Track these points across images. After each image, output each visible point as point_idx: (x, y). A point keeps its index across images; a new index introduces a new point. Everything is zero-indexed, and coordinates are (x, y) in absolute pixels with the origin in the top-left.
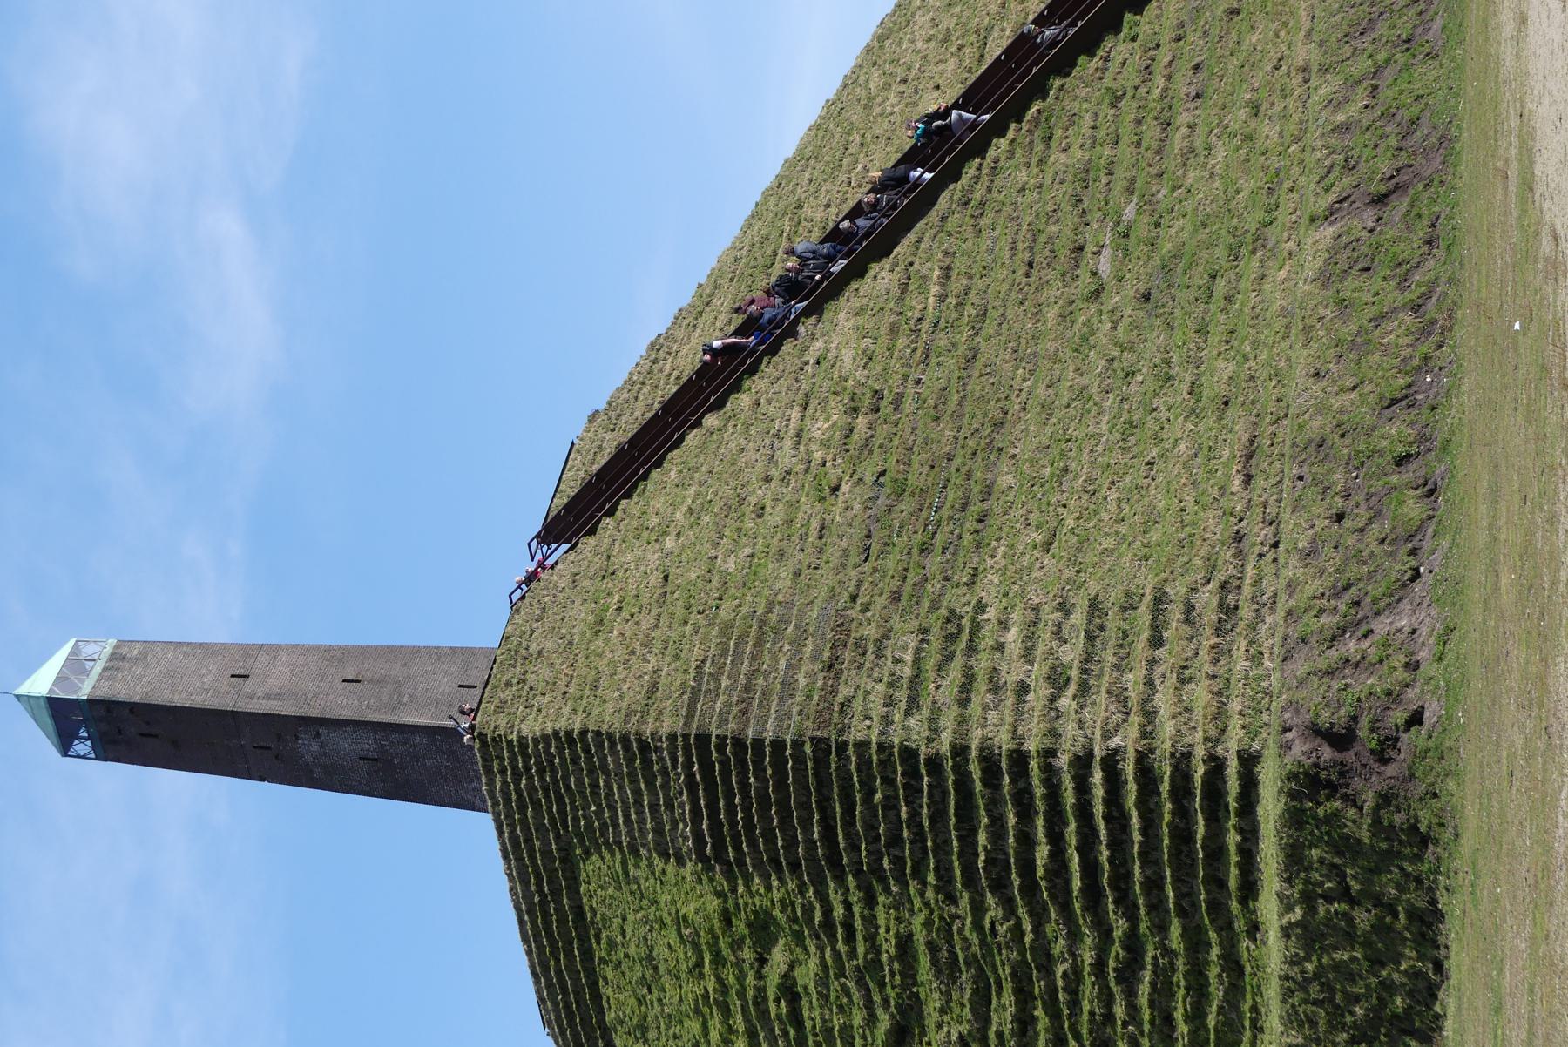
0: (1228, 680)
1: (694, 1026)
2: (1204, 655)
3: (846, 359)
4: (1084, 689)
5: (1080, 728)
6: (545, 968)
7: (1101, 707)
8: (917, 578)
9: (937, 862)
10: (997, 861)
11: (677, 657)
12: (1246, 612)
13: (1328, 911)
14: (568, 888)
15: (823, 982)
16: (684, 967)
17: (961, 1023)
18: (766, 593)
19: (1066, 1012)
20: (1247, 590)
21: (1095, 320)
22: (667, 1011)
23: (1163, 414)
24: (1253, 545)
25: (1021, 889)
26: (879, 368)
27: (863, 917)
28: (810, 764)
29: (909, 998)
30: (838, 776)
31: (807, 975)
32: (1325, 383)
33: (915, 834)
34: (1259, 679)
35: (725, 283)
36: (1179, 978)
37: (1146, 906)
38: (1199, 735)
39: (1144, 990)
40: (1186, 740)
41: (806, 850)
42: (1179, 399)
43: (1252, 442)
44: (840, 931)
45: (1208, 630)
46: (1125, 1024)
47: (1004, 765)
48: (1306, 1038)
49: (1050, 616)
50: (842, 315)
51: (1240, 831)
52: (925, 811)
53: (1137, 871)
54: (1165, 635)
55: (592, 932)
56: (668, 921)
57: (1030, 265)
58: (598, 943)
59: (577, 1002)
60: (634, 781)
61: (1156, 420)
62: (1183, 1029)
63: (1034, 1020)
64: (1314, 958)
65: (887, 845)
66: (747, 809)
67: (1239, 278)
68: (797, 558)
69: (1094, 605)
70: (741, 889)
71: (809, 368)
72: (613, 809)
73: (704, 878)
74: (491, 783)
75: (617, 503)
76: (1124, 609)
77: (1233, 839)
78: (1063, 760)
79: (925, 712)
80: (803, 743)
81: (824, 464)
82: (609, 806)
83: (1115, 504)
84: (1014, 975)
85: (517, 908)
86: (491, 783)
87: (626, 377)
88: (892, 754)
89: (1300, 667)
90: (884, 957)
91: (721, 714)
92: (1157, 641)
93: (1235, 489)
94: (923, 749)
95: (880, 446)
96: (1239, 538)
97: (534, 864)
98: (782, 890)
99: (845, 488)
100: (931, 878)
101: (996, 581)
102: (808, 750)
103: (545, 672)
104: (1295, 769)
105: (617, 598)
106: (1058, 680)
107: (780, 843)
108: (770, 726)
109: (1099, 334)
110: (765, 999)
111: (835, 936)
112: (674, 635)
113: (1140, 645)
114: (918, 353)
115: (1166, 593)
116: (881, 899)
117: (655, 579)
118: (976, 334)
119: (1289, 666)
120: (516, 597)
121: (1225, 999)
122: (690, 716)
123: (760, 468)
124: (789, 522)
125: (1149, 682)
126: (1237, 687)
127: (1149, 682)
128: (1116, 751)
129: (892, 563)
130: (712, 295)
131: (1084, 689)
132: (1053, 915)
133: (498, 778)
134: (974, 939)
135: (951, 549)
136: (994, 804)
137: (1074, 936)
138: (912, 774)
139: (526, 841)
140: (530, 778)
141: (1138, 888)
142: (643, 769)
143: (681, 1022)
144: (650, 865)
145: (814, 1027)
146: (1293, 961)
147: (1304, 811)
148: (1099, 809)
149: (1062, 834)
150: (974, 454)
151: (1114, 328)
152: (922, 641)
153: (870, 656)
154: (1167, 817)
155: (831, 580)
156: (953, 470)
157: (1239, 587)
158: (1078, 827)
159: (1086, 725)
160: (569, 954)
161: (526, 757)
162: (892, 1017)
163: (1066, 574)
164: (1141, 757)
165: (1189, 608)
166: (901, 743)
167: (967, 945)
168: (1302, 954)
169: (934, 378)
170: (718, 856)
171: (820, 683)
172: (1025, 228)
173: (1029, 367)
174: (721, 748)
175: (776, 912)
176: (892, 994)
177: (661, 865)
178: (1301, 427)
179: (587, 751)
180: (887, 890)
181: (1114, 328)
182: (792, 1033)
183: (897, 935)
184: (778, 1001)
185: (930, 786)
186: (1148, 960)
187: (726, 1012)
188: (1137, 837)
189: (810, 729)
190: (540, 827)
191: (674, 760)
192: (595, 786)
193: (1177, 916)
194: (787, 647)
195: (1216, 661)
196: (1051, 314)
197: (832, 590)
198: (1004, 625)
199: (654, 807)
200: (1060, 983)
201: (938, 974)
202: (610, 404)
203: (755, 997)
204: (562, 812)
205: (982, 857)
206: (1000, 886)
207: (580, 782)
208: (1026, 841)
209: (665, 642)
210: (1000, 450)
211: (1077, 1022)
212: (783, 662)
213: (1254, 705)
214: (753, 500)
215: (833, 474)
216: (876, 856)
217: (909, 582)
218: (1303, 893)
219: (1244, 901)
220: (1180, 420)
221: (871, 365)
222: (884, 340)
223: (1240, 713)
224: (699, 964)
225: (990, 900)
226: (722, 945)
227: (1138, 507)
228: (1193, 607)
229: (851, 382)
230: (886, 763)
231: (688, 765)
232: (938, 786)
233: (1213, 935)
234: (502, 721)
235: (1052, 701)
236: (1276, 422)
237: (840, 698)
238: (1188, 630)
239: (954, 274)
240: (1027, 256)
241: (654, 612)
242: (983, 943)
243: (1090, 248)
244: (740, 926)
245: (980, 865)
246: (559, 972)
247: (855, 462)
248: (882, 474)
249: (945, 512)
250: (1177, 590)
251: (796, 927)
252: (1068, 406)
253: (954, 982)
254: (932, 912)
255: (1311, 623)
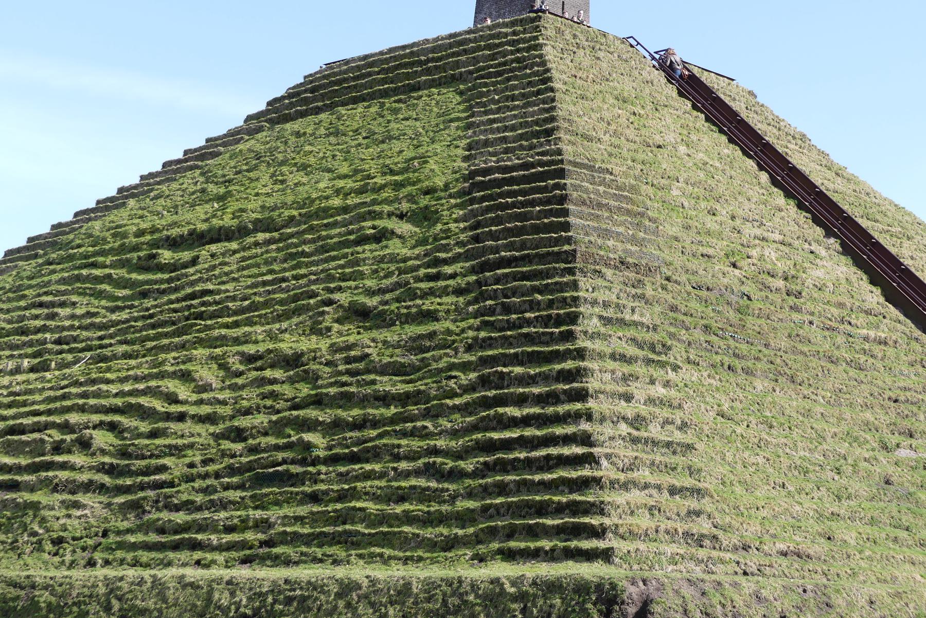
0: (656, 540)
1: (345, 169)
2: (670, 524)
3: (818, 272)
4: (635, 441)
5: (610, 438)
6: (371, 65)
7: (627, 453)
8: (687, 323)
9: (496, 339)
10: (502, 380)
11: (610, 155)
12: (702, 553)
13: (515, 610)
14: (433, 80)
15: (393, 259)
16: (388, 162)
17: (378, 355)
18: (662, 217)
19: (398, 428)
20: (715, 554)
21: (868, 446)
22: (353, 150)
23: (816, 494)
24: (744, 558)
25: (484, 397)
26: (815, 295)
27: (447, 287)
28: (556, 249)
29: (391, 319)
30: (550, 269)
31: (395, 247)
32: (868, 608)
33: (514, 323)
34: (659, 562)
35: (852, 186)
36: (434, 507)
37: (486, 484)
38: (616, 520)
39: (422, 482)
40: (613, 512)
41: (491, 247)
42: (828, 506)
43: (808, 556)
44: (434, 271)
45: (686, 527)
46: (395, 469)
47: (575, 385)
48: (417, 594)
49: (678, 416)
50: (845, 269)
51: (553, 550)
52: (534, 330)
53: (510, 477)
54: (677, 497)
55: (403, 97)
56: (421, 150)
57: (896, 401)
58: (395, 102)
59: (349, 87)
60: (521, 125)
61: (812, 489)
62: (399, 509)
63: (387, 406)
64: (478, 601)
65: (503, 304)
66: (514, 206)
67: (908, 547)
68: (687, 239)
69: (690, 447)
70: (453, 201)
71: (806, 246)
72: (498, 111)
73: (458, 175)
74: (505, 25)
75: (702, 112)
76: (689, 468)
77: (546, 544)
78: (585, 426)
79: (603, 330)
80: (570, 244)
81: (748, 257)
82: (500, 108)
83: (755, 461)
84: (419, 392)
85: (414, 45)
86: (505, 25)
87: (781, 117)
88: (571, 306)
89: (688, 592)
90: (419, 302)
91: (580, 186)
92: (673, 491)
93: (777, 545)
94: (579, 328)
95: (767, 297)
96: (746, 548)
97: (448, 56)
98: (457, 230)
99: (737, 272)
100: (483, 334)
101: (693, 379)
102: (566, 248)
103: (586, 62)
104: (619, 588)
105: (642, 112)
106: (637, 422)
107: (493, 228)
108: (578, 221)
109: (860, 450)
110: (374, 219)
111: (429, 267)
112: (625, 152)
113: (667, 480)
114: (829, 323)
115: (703, 497)
116: (461, 299)
117: (658, 139)
118: (847, 363)
119: (686, 584)
120: (631, 40)
121: (424, 539)
122: (576, 164)
123: (740, 212)
124: (708, 233)
125: (646, 486)
126: (653, 546)
127: (646, 486)
128: (597, 463)
129: (694, 305)
130: (843, 177)
131: (635, 441)
132: (468, 419)
133: (509, 30)
134: (442, 364)
135: (709, 347)
136: (545, 378)
137: (454, 434)
138: (559, 321)
139: (465, 50)
140: (512, 53)
141: (498, 478)
142: (532, 132)
143: (346, 160)
144: (460, 138)
145: (358, 253)
146: (474, 586)
147: (588, 594)
148: (554, 451)
149: (530, 425)
150: (772, 363)
151: (865, 460)
152: (648, 327)
153: (633, 291)
154: (556, 499)
155: (678, 263)
156: (760, 348)
157: (714, 548)
158: (538, 437)
159: (612, 443)
160: (384, 81)
161: (528, 49)
162: (376, 308)
163: (706, 428)
164: (597, 481)
165: (698, 513)
166: (581, 313)
167: (437, 359)
168: (480, 592)
169: (816, 334)
170: (475, 185)
171: (611, 256)
172: (920, 397)
173: (832, 400)
174: (557, 186)
175: (439, 227)
176: (394, 306)
177: (462, 145)
178: (838, 591)
179: (539, 92)
180: (469, 303)
181: (865, 460)
182: (352, 237)
183: (437, 311)
184: (374, 227)
185: (552, 333)
186: (446, 485)
187: (361, 191)
188: (537, 478)
189: (581, 248)
190: (476, 60)
191: (543, 154)
192: (513, 98)
193: (483, 506)
194: (631, 233)
195: (667, 532)
196: (868, 415)
197: (671, 264)
198: (667, 384)
199: (504, 140)
200: (419, 424)
201: (414, 339)
202: (762, 106)
203: (375, 212)
204: (489, 76)
205: (505, 370)
206: (484, 382)
207: (514, 88)
208: (521, 401)
209: (619, 147)
210: (777, 381)
211: (391, 435)
212: (621, 229)
213: (643, 559)
214: (718, 207)
215: (742, 263)
216: (494, 296)
217: (684, 318)
218: (527, 593)
219: (500, 552)
220: (815, 507)
221: (816, 290)
222: (834, 299)
223: (638, 549)
224: (392, 172)
225: (473, 376)
226: (409, 188)
227: (755, 478)
228: (698, 516)
229: (804, 275)
230: (564, 302)
231: (541, 164)
232: (552, 339)
233: (471, 530)
234: (550, 32)
235: (623, 418)
236: (824, 573)
237: (604, 270)
238: (683, 513)
239: (882, 347)
240: (902, 398)
241: (637, 139)
242: (440, 371)
243: (914, 442)
244: (424, 201)
245: (499, 369)
246: (369, 74)
247: (754, 279)
248: (749, 298)
249: (732, 342)
250: (706, 504)
251: (430, 240)
252: (812, 428)
253: (407, 350)
254: (457, 335)
255: (716, 599)
